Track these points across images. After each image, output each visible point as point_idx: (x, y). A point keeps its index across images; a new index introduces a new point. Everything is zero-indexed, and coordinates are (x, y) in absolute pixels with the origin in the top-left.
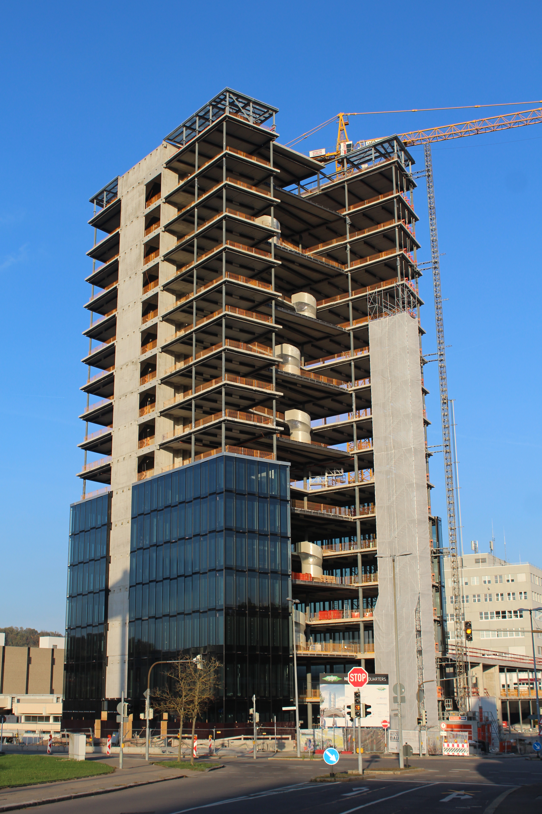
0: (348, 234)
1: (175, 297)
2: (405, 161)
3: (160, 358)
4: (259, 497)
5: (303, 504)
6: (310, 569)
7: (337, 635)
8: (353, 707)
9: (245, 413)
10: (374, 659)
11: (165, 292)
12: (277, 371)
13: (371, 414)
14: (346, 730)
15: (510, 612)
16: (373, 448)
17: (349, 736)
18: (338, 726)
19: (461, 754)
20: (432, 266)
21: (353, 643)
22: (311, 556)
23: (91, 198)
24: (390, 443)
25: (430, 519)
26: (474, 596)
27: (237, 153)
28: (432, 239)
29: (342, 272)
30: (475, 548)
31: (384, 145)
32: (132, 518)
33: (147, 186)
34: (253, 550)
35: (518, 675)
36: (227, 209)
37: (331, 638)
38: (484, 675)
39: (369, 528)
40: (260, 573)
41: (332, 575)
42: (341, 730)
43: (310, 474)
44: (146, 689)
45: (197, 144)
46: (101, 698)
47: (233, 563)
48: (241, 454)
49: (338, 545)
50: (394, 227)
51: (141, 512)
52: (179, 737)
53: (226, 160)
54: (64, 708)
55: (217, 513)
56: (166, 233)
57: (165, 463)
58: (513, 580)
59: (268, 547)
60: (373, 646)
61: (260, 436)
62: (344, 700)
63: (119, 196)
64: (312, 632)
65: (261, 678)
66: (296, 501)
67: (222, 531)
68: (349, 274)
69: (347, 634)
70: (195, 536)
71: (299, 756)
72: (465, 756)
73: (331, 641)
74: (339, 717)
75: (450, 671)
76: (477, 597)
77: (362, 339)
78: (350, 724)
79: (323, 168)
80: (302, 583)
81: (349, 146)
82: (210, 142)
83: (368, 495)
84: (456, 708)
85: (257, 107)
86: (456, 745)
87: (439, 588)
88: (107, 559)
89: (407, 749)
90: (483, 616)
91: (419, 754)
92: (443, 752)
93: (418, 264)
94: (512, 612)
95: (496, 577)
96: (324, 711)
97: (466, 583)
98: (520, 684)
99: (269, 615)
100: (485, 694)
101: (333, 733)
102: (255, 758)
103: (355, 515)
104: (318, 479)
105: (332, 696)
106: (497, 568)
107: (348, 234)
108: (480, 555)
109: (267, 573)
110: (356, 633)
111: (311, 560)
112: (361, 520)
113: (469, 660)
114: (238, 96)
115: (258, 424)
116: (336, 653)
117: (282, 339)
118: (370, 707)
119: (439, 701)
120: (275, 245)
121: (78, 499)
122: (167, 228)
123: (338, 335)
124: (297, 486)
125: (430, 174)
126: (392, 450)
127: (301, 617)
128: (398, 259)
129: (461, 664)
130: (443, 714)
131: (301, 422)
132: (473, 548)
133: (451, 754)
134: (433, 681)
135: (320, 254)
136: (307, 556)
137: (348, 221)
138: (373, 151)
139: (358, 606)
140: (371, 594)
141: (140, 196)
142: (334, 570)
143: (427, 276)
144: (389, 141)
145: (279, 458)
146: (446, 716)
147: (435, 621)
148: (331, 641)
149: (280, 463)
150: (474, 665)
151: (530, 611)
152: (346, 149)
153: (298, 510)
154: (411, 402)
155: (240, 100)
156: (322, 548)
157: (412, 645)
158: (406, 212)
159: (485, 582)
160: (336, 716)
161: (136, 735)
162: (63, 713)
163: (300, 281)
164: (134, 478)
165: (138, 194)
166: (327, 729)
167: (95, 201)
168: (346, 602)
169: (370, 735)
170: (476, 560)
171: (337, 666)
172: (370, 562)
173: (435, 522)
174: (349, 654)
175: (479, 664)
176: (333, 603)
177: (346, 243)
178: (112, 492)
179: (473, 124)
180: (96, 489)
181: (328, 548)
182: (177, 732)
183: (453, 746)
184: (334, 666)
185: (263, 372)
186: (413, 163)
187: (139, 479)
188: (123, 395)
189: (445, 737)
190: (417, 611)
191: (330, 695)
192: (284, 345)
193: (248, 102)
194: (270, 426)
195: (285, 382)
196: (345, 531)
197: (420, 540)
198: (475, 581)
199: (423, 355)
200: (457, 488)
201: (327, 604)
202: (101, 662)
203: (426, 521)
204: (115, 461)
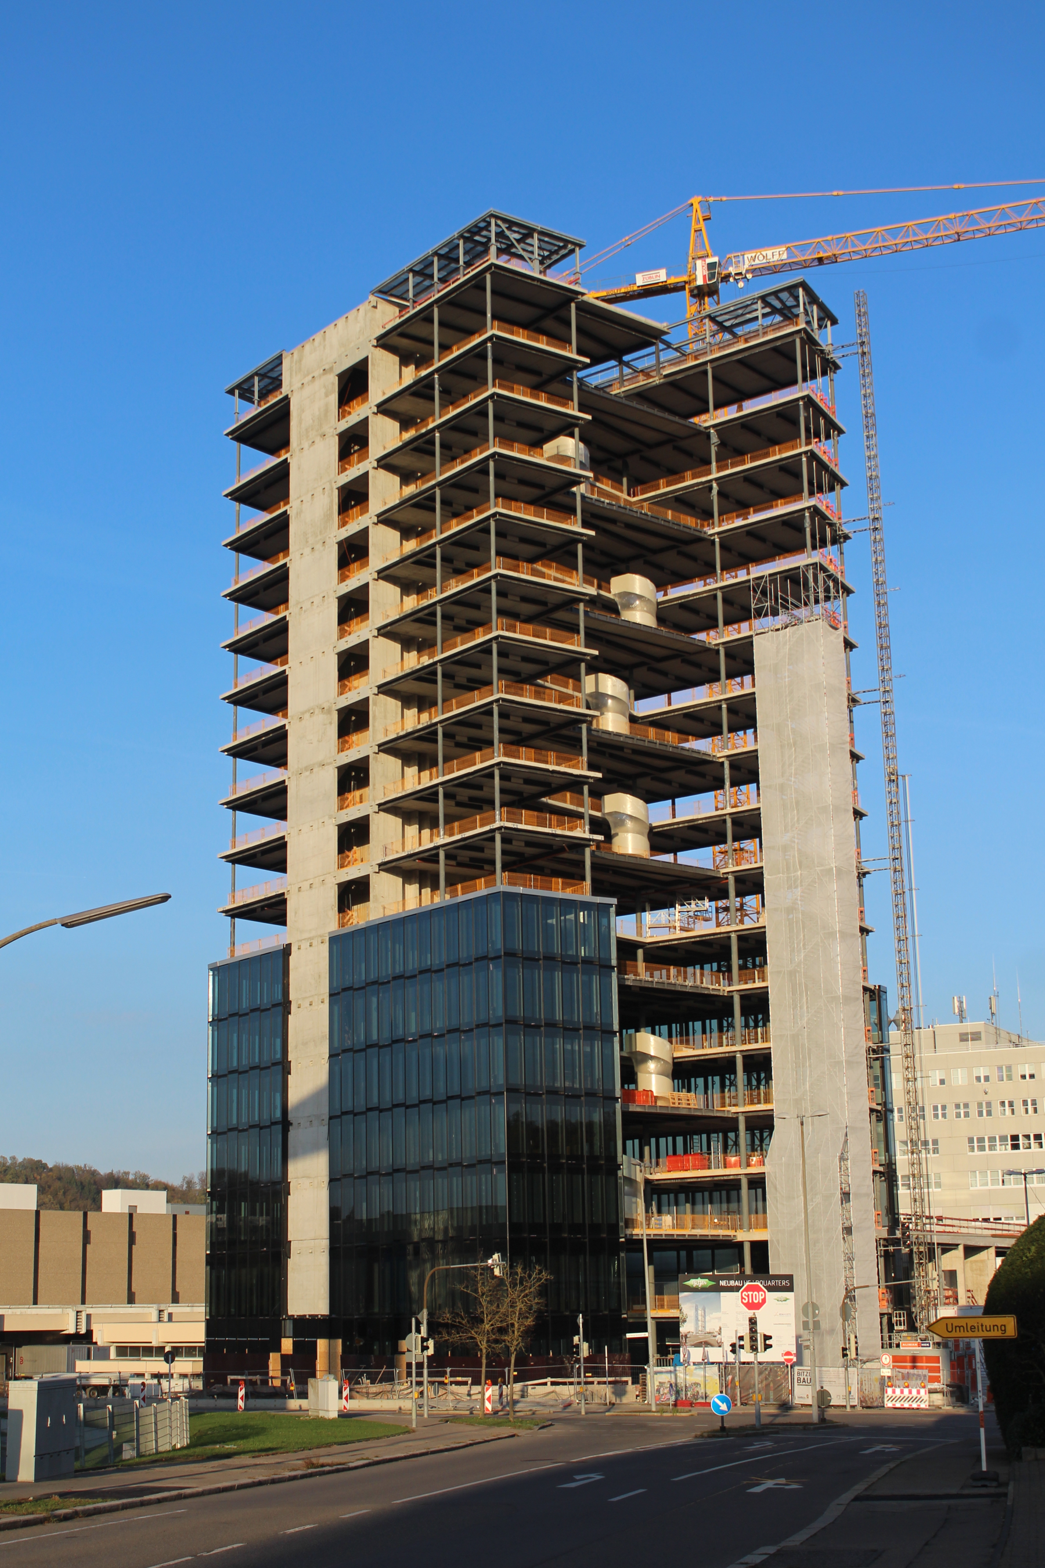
0: (714, 464)
1: (398, 590)
2: (818, 320)
3: (375, 704)
4: (564, 963)
5: (636, 967)
7: (699, 1196)
8: (747, 1339)
9: (536, 813)
10: (766, 1242)
11: (381, 581)
12: (589, 730)
13: (754, 686)
14: (725, 1368)
15: (1028, 1137)
16: (763, 864)
17: (730, 1377)
18: (711, 1360)
19: (915, 1405)
20: (867, 524)
21: (728, 1212)
22: (652, 1058)
23: (229, 386)
24: (794, 856)
25: (865, 989)
26: (958, 1106)
27: (512, 333)
28: (869, 474)
29: (702, 535)
30: (961, 1011)
31: (781, 295)
32: (331, 995)
33: (341, 376)
34: (554, 1051)
36: (497, 439)
37: (687, 1201)
38: (968, 1265)
39: (757, 1006)
40: (567, 1096)
41: (689, 1091)
42: (715, 1368)
43: (648, 907)
44: (422, 1309)
45: (436, 310)
46: (280, 1315)
47: (519, 1080)
49: (699, 1036)
50: (800, 454)
51: (348, 984)
52: (446, 1381)
53: (492, 347)
54: (208, 1333)
55: (492, 992)
56: (381, 471)
57: (392, 899)
58: (1032, 1076)
59: (580, 1046)
60: (765, 1219)
61: (562, 850)
62: (719, 1318)
63: (285, 390)
64: (660, 1195)
65: (593, 1292)
66: (628, 962)
67: (500, 1025)
68: (717, 540)
69: (716, 1194)
70: (449, 1031)
71: (654, 1409)
72: (923, 1409)
73: (688, 1206)
74: (712, 1346)
75: (901, 1261)
76: (963, 1108)
77: (741, 660)
78: (731, 1357)
79: (665, 333)
80: (639, 1109)
81: (711, 266)
82: (461, 311)
83: (754, 947)
85: (546, 239)
86: (906, 1391)
87: (882, 1114)
88: (284, 1067)
89: (823, 1396)
90: (976, 1144)
92: (886, 1400)
93: (843, 521)
95: (1000, 1068)
96: (686, 1336)
97: (942, 1082)
99: (583, 1169)
101: (702, 1373)
102: (583, 1413)
104: (662, 915)
106: (1006, 1050)
107: (714, 464)
108: (969, 1026)
109: (579, 1097)
110: (734, 1193)
111: (652, 1065)
113: (936, 1240)
114: (511, 224)
115: (559, 832)
116: (698, 1232)
117: (595, 667)
118: (770, 1337)
119: (882, 1315)
120: (583, 497)
121: (223, 957)
122: (383, 462)
123: (695, 653)
124: (625, 927)
125: (866, 350)
126: (796, 871)
127: (638, 1169)
128: (807, 514)
129: (922, 1249)
130: (890, 1338)
131: (631, 816)
132: (957, 1011)
133: (898, 1405)
135: (662, 502)
136: (646, 1057)
137: (715, 439)
138: (760, 304)
139: (736, 1144)
140: (762, 1126)
141: (327, 395)
142: (693, 1080)
143: (857, 548)
144: (791, 289)
145: (595, 892)
146: (895, 1342)
147: (875, 1172)
148: (688, 1206)
149: (599, 900)
150: (947, 1248)
151: (1025, 1174)
152: (706, 273)
153: (630, 979)
154: (829, 781)
155: (514, 229)
156: (671, 1043)
157: (833, 1216)
158: (822, 422)
159: (978, 1079)
160: (707, 1344)
161: (364, 1380)
162: (208, 1342)
163: (625, 551)
164: (332, 924)
165: (323, 391)
166: (692, 1367)
167: (237, 392)
168: (714, 1136)
169: (763, 1375)
170: (961, 1035)
171: (700, 1252)
172: (759, 1066)
173: (875, 995)
174: (721, 1232)
175: (957, 1245)
176: (691, 1139)
177: (711, 481)
178: (289, 945)
179: (948, 222)
180: (258, 938)
181: (681, 1043)
182: (443, 1374)
183: (902, 1392)
184: (695, 1252)
185: (565, 732)
186: (834, 322)
187: (342, 925)
188: (306, 770)
189: (889, 1377)
190: (842, 1159)
191: (697, 1310)
192: (600, 675)
193: (528, 232)
194: (578, 833)
195: (605, 749)
196: (713, 1010)
197: (848, 1031)
198: (960, 1078)
199: (853, 691)
200: (914, 936)
201: (680, 1140)
202: (274, 1249)
203: (858, 999)
204: (294, 889)
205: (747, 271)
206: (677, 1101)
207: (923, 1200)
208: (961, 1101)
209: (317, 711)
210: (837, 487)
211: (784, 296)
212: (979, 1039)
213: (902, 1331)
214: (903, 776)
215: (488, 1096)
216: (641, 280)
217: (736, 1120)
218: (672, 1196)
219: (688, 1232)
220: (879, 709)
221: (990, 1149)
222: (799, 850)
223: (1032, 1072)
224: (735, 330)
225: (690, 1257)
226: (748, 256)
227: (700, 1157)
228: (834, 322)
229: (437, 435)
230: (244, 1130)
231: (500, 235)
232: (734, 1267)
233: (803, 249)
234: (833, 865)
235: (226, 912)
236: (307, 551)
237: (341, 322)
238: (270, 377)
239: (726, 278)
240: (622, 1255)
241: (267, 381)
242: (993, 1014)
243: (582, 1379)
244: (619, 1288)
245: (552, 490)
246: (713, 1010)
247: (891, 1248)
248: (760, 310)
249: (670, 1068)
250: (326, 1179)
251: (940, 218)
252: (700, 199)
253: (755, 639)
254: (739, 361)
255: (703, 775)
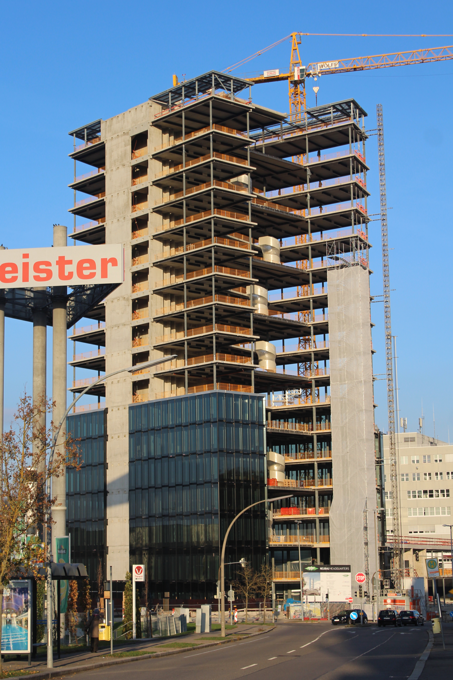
3: (152, 299)
4: (243, 424)
6: (275, 474)
15: (437, 491)
21: (307, 534)
22: (275, 463)
28: (381, 194)
37: (287, 528)
48: (229, 390)
57: (160, 391)
58: (440, 461)
62: (320, 583)
68: (309, 221)
73: (288, 530)
81: (302, 71)
82: (197, 117)
84: (392, 586)
88: (105, 466)
90: (411, 494)
91: (373, 621)
94: (440, 491)
95: (424, 457)
98: (445, 560)
100: (415, 574)
103: (312, 430)
108: (409, 434)
112: (318, 435)
114: (220, 76)
125: (381, 133)
129: (397, 552)
137: (309, 173)
138: (332, 108)
140: (327, 496)
144: (348, 103)
146: (384, 593)
148: (288, 530)
150: (407, 550)
151: (451, 526)
158: (360, 166)
159: (413, 461)
161: (161, 609)
164: (129, 401)
167: (74, 135)
170: (405, 438)
171: (293, 551)
173: (378, 436)
175: (410, 549)
184: (291, 552)
188: (115, 326)
191: (310, 580)
193: (229, 79)
196: (304, 441)
200: (397, 411)
205: (319, 73)
206: (287, 483)
207: (398, 530)
208: (405, 473)
209: (121, 299)
210: (365, 197)
211: (344, 106)
212: (414, 441)
213: (387, 589)
214: (394, 337)
215: (210, 484)
216: (266, 74)
217: (314, 492)
218: (280, 525)
219: (288, 544)
220: (383, 305)
221: (419, 497)
222: (347, 372)
223: (440, 459)
224: (319, 117)
225: (288, 554)
226: (319, 64)
227: (297, 509)
228: (365, 115)
229: (184, 174)
230: (83, 495)
231: (216, 79)
232: (309, 559)
233: (347, 63)
234: (362, 379)
235: (72, 390)
236: (115, 221)
237: (133, 111)
238: (93, 131)
239: (308, 75)
240: (267, 554)
241: (90, 130)
242: (420, 427)
243: (260, 609)
245: (237, 204)
246: (304, 441)
247: (383, 551)
248: (332, 110)
249: (284, 468)
250: (128, 519)
251: (414, 51)
252: (296, 33)
253: (328, 272)
254: (322, 135)
255: (299, 331)
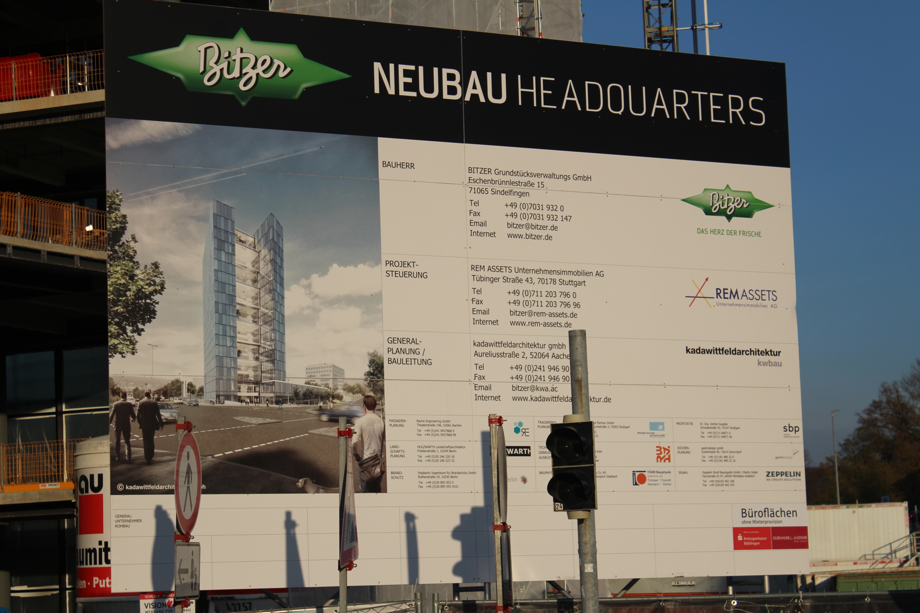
35: (587, 551)
62: (370, 304)
105: (244, 256)
134: (290, 525)
244: (178, 475)
